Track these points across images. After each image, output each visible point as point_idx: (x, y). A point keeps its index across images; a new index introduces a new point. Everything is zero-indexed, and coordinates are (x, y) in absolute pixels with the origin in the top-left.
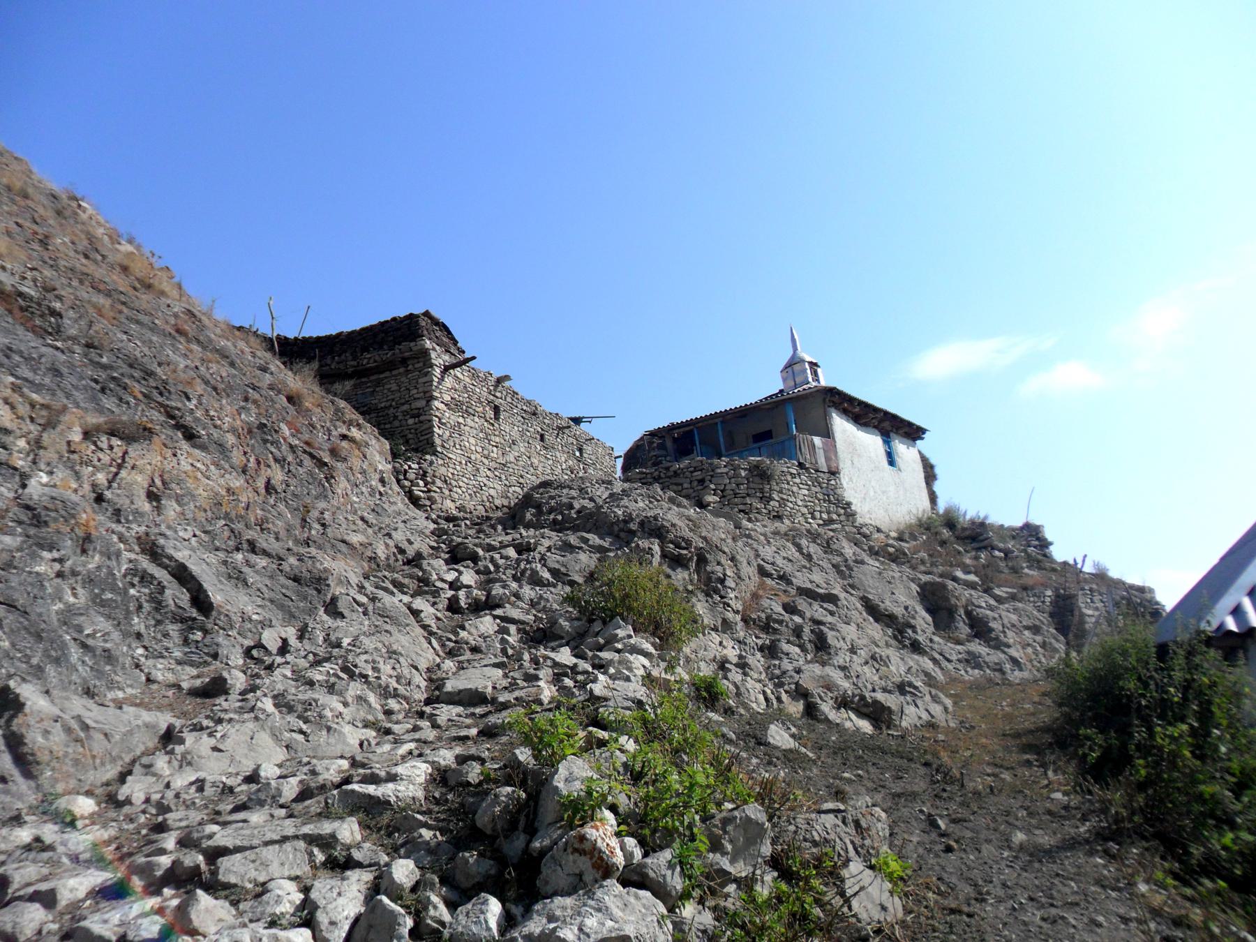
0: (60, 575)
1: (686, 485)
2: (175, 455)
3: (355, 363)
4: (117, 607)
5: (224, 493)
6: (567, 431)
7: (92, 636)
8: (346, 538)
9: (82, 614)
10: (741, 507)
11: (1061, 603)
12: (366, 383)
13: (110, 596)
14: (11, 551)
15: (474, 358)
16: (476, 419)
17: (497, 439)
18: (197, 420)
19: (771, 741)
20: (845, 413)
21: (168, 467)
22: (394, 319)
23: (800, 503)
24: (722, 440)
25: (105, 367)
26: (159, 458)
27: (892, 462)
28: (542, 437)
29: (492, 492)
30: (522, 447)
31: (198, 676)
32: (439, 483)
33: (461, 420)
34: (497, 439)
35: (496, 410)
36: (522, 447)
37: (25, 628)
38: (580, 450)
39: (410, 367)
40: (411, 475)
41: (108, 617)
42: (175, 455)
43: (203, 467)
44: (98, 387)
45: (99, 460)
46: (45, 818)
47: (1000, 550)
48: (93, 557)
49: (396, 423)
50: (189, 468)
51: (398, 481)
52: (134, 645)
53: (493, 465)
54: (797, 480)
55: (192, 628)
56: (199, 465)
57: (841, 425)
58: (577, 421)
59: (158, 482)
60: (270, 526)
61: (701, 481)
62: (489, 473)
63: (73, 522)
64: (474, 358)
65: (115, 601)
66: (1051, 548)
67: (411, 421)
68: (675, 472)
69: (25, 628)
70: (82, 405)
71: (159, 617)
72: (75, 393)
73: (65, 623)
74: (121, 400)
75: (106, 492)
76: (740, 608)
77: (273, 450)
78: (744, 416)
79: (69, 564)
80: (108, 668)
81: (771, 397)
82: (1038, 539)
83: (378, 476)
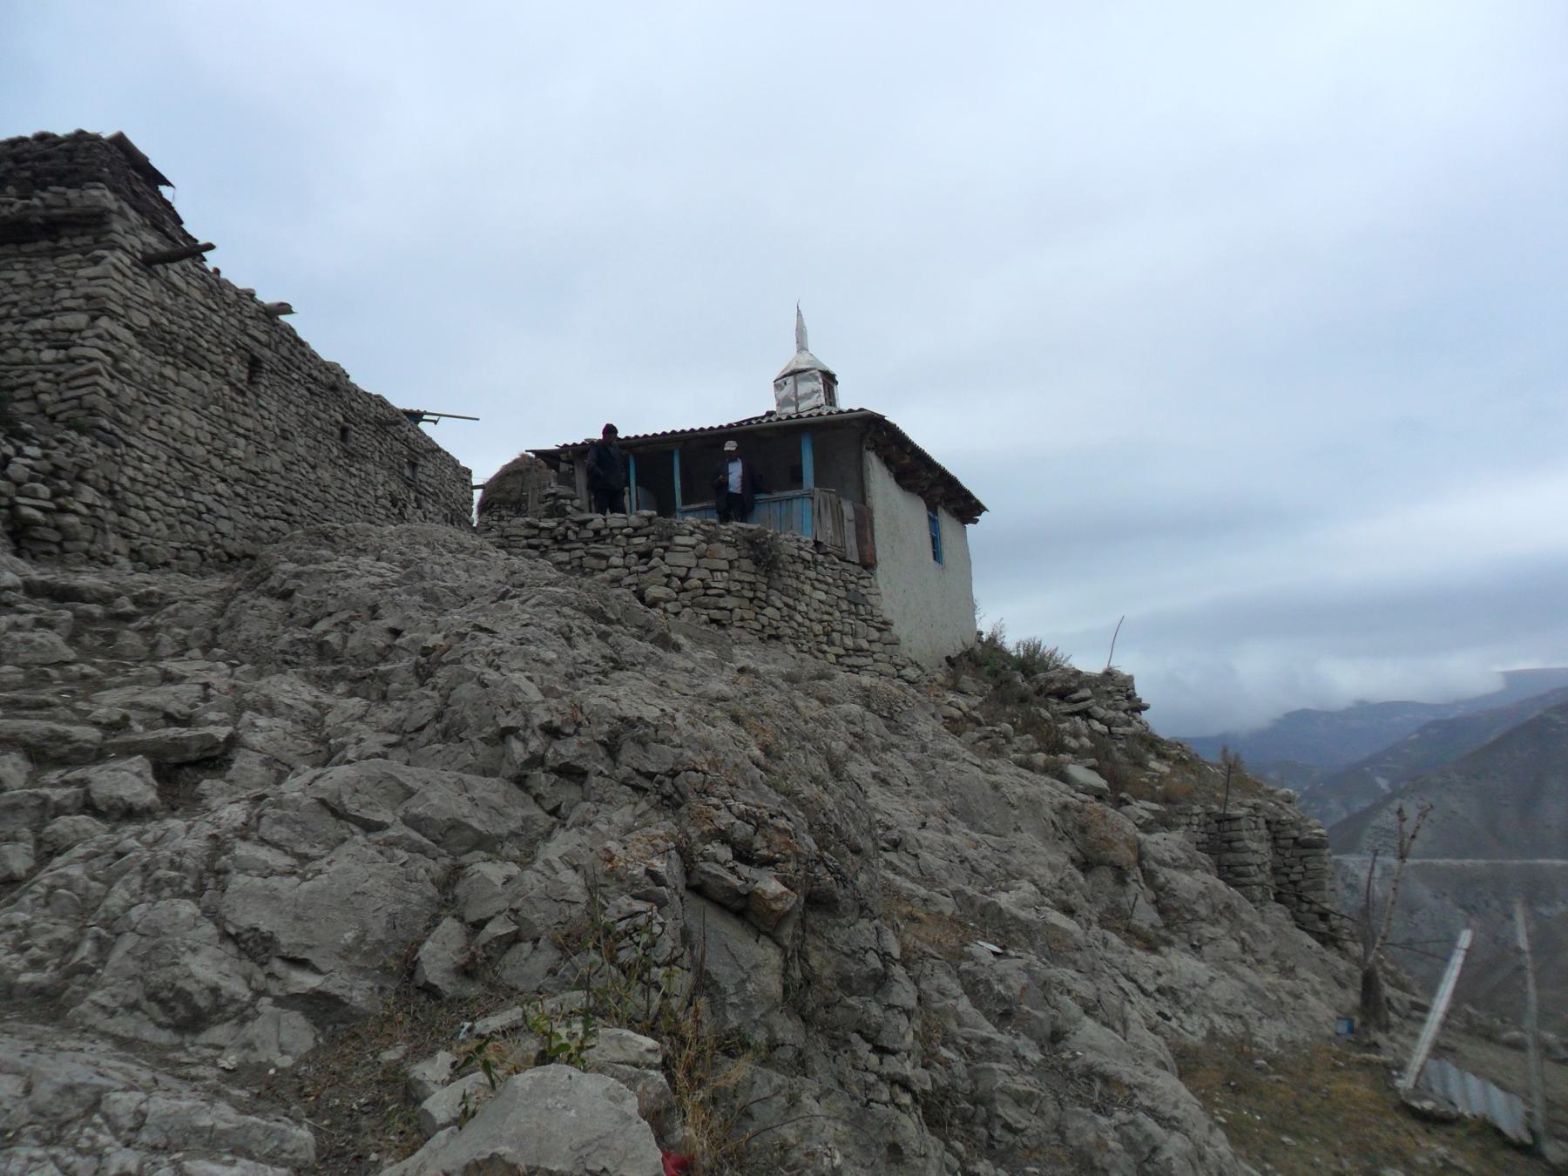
6: (392, 429)
10: (716, 614)
11: (1214, 827)
16: (207, 377)
17: (249, 423)
20: (887, 461)
22: (42, 137)
23: (813, 615)
24: (1516, 862)
27: (937, 556)
28: (344, 431)
29: (225, 526)
30: (300, 445)
32: (88, 495)
33: (169, 372)
35: (254, 364)
36: (300, 445)
38: (413, 466)
39: (64, 242)
47: (1101, 721)
53: (233, 471)
54: (812, 574)
57: (880, 482)
58: (416, 416)
61: (645, 555)
62: (221, 487)
66: (212, 260)
67: (48, 355)
68: (597, 532)
81: (739, 424)
82: (1129, 697)
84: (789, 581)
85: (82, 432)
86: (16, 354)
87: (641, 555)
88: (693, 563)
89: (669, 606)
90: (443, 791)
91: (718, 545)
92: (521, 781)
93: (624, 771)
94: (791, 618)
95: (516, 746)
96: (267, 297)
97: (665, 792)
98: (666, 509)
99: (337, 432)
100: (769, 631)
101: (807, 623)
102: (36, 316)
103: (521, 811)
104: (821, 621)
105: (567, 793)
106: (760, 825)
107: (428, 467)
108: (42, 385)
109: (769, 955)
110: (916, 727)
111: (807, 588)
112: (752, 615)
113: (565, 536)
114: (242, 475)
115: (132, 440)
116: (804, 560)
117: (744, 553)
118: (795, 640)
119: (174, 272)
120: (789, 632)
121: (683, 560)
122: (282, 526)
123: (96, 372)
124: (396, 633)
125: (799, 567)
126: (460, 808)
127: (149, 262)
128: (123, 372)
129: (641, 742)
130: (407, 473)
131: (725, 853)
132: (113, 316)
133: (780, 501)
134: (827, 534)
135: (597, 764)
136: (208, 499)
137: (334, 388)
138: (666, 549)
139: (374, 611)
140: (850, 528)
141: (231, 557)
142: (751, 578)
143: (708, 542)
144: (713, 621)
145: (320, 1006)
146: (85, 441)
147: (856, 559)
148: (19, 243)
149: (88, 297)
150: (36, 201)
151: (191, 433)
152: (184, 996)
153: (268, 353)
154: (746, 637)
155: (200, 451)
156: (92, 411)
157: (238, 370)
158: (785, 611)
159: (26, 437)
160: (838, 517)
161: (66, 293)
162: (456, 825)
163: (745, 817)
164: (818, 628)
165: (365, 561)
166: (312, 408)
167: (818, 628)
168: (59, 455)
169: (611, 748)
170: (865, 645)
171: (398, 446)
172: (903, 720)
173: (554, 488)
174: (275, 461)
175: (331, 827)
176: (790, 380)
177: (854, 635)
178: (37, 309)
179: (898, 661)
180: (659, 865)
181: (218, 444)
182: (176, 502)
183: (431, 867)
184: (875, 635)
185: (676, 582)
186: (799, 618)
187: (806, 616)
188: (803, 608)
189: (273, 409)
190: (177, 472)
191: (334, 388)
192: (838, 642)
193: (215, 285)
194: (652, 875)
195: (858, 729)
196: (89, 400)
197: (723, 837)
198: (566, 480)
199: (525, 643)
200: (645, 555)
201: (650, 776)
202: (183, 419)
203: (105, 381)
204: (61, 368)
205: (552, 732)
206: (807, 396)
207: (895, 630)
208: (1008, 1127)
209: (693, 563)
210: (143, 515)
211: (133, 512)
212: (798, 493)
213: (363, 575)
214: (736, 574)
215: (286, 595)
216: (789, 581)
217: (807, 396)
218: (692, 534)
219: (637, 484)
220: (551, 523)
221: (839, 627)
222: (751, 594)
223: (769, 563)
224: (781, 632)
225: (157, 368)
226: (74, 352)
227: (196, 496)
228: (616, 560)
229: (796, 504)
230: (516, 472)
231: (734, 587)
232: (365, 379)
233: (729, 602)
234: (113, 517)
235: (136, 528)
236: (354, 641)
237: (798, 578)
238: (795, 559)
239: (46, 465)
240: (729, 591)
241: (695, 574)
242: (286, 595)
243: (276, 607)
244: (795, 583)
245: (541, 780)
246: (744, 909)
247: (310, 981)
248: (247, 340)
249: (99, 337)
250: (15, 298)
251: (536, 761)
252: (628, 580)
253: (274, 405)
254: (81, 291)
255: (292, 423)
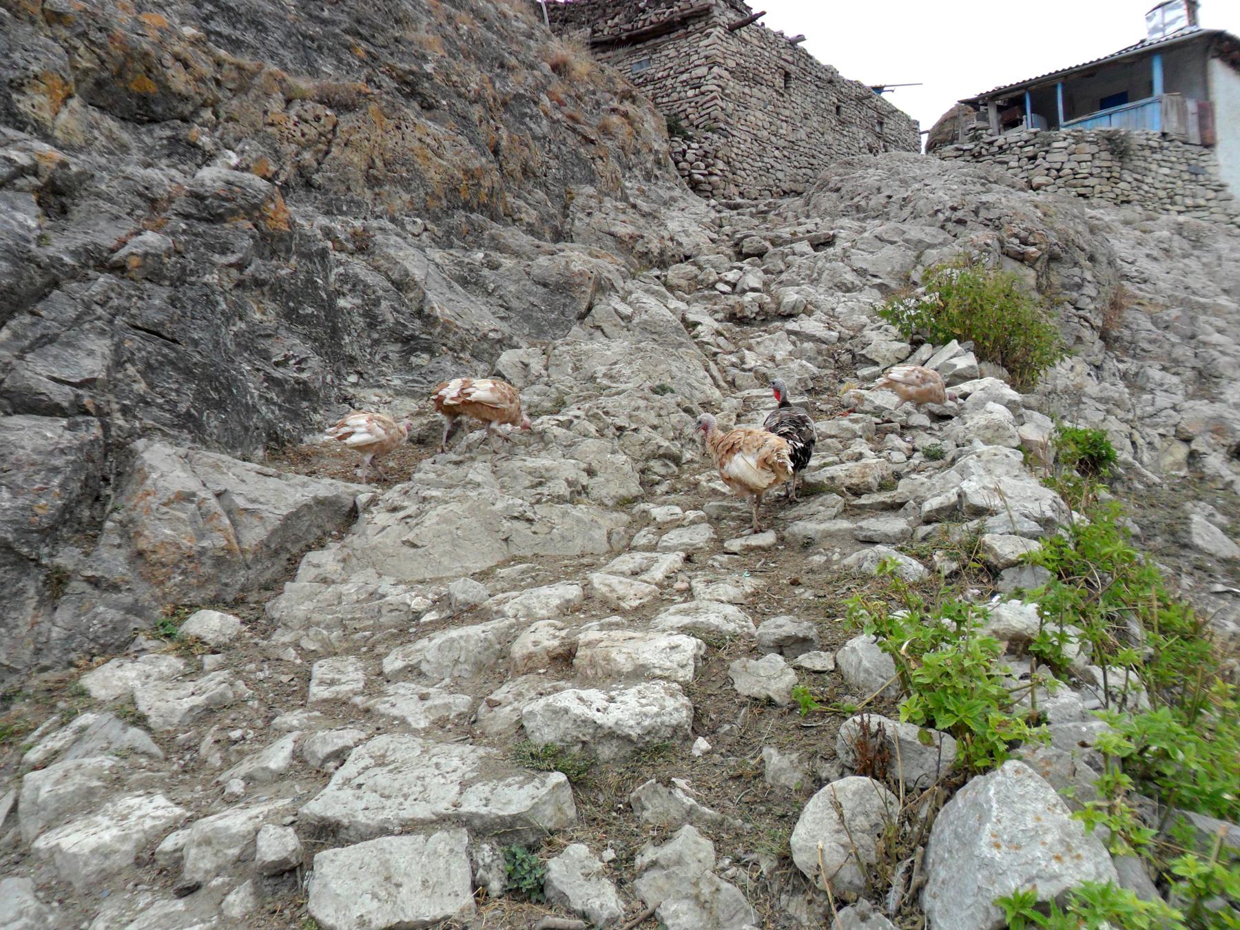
0: (240, 285)
1: (1012, 164)
2: (398, 128)
3: (629, 26)
4: (318, 324)
5: (461, 176)
7: (283, 363)
8: (613, 229)
9: (269, 336)
10: (1082, 191)
12: (641, 50)
13: (309, 310)
14: (158, 256)
15: (763, 13)
16: (765, 89)
17: (787, 113)
18: (436, 87)
19: (1198, 541)
21: (390, 145)
23: (1158, 185)
25: (323, 22)
26: (379, 132)
28: (838, 108)
29: (780, 175)
30: (814, 121)
31: (419, 414)
32: (720, 165)
33: (747, 90)
34: (787, 113)
35: (787, 76)
37: (171, 363)
38: (881, 124)
39: (691, 28)
40: (690, 156)
41: (307, 337)
42: (398, 128)
43: (433, 143)
44: (315, 46)
45: (303, 135)
46: (169, 645)
48: (287, 260)
49: (675, 96)
50: (417, 144)
51: (677, 163)
52: (343, 371)
53: (782, 143)
54: (1158, 156)
55: (416, 350)
56: (428, 140)
58: (879, 89)
59: (379, 163)
60: (523, 216)
61: (1033, 158)
62: (777, 153)
63: (257, 214)
64: (763, 13)
65: (317, 317)
67: (691, 93)
68: (1000, 147)
69: (171, 363)
70: (290, 66)
71: (376, 336)
72: (281, 51)
73: (246, 348)
74: (340, 61)
75: (315, 176)
76: (1100, 324)
77: (532, 126)
78: (1092, 75)
79: (249, 270)
80: (305, 404)
81: (1120, 53)
83: (652, 157)
84: (1138, 163)
85: (713, 131)
86: (675, 96)
87: (1030, 158)
88: (1065, 158)
89: (1049, 188)
90: (915, 231)
91: (1084, 144)
92: (943, 227)
93: (981, 219)
94: (1139, 188)
95: (940, 215)
96: (790, 34)
97: (994, 224)
98: (1052, 124)
99: (834, 109)
100: (1121, 198)
101: (1153, 190)
102: (682, 73)
103: (942, 236)
104: (1165, 189)
105: (960, 229)
106: (1031, 233)
107: (890, 124)
108: (690, 110)
109: (1032, 273)
110: (1216, 245)
111: (1154, 167)
112: (1109, 188)
113: (980, 153)
114: (786, 144)
115: (734, 133)
116: (1151, 148)
117: (1103, 148)
118: (1142, 203)
119: (744, 32)
120: (1137, 197)
121: (1056, 158)
122: (809, 172)
123: (714, 98)
124: (890, 197)
125: (1147, 153)
126: (922, 236)
127: (732, 29)
128: (728, 95)
129: (988, 209)
130: (878, 129)
131: (1017, 241)
132: (720, 65)
133: (1136, 107)
134: (1173, 127)
135: (970, 218)
136: (771, 161)
137: (830, 82)
138: (1047, 152)
139: (879, 189)
140: (1193, 120)
141: (785, 192)
142: (1109, 164)
143: (1076, 143)
144: (1080, 195)
145: (882, 288)
146: (716, 136)
147: (1197, 141)
148: (669, 33)
149: (707, 57)
150: (676, 9)
151: (760, 124)
152: (844, 284)
153: (793, 67)
154: (1103, 203)
155: (765, 133)
156: (716, 120)
157: (779, 82)
158: (1135, 184)
159: (690, 138)
160: (1182, 114)
161: (696, 57)
162: (920, 241)
163: (1025, 229)
164: (1162, 194)
165: (871, 171)
166: (819, 97)
167: (1162, 194)
168: (706, 146)
169: (976, 212)
170: (1202, 202)
171: (870, 112)
172: (1206, 241)
173: (975, 124)
174: (802, 134)
175: (879, 244)
176: (1159, 11)
177: (1194, 196)
178: (682, 69)
179: (1229, 211)
180: (989, 241)
181: (773, 128)
182: (757, 164)
183: (912, 254)
184: (1211, 194)
185: (1054, 173)
186: (1146, 188)
187: (1152, 186)
188: (1149, 180)
189: (799, 102)
190: (756, 147)
191: (830, 82)
192: (1179, 202)
193: (764, 34)
194: (987, 245)
195: (1165, 246)
196: (713, 114)
197: (1016, 236)
198: (983, 117)
199: (945, 182)
200: (1033, 158)
201: (990, 220)
202: (757, 117)
203: (719, 102)
204: (697, 99)
205: (954, 209)
206: (1173, 22)
207: (1229, 190)
208: (1143, 350)
209: (1065, 158)
210: (743, 173)
211: (739, 172)
212: (1149, 100)
213: (872, 177)
214: (1097, 163)
215: (838, 190)
216: (1138, 163)
217: (1173, 22)
218: (1065, 139)
219: (1032, 112)
220: (971, 146)
221: (1181, 192)
222: (1108, 175)
223: (1121, 152)
224: (1130, 198)
225: (742, 89)
226: (703, 89)
227: (766, 160)
228: (1012, 164)
229: (1149, 108)
230: (950, 119)
231: (1095, 171)
232: (847, 72)
233: (1091, 181)
234: (730, 176)
235: (741, 180)
236: (871, 203)
237: (1145, 160)
238: (1143, 147)
239: (701, 152)
240: (1091, 175)
241: (1067, 166)
242: (838, 190)
243: (835, 195)
244: (1143, 164)
245: (950, 226)
246: (1021, 258)
247: (879, 281)
248: (782, 62)
249: (714, 78)
250: (670, 65)
251: (948, 220)
252: (1022, 175)
253: (800, 99)
254: (702, 54)
255: (809, 108)
